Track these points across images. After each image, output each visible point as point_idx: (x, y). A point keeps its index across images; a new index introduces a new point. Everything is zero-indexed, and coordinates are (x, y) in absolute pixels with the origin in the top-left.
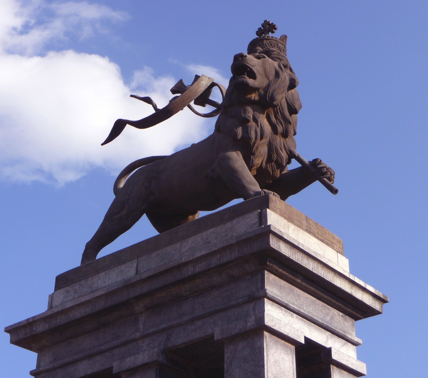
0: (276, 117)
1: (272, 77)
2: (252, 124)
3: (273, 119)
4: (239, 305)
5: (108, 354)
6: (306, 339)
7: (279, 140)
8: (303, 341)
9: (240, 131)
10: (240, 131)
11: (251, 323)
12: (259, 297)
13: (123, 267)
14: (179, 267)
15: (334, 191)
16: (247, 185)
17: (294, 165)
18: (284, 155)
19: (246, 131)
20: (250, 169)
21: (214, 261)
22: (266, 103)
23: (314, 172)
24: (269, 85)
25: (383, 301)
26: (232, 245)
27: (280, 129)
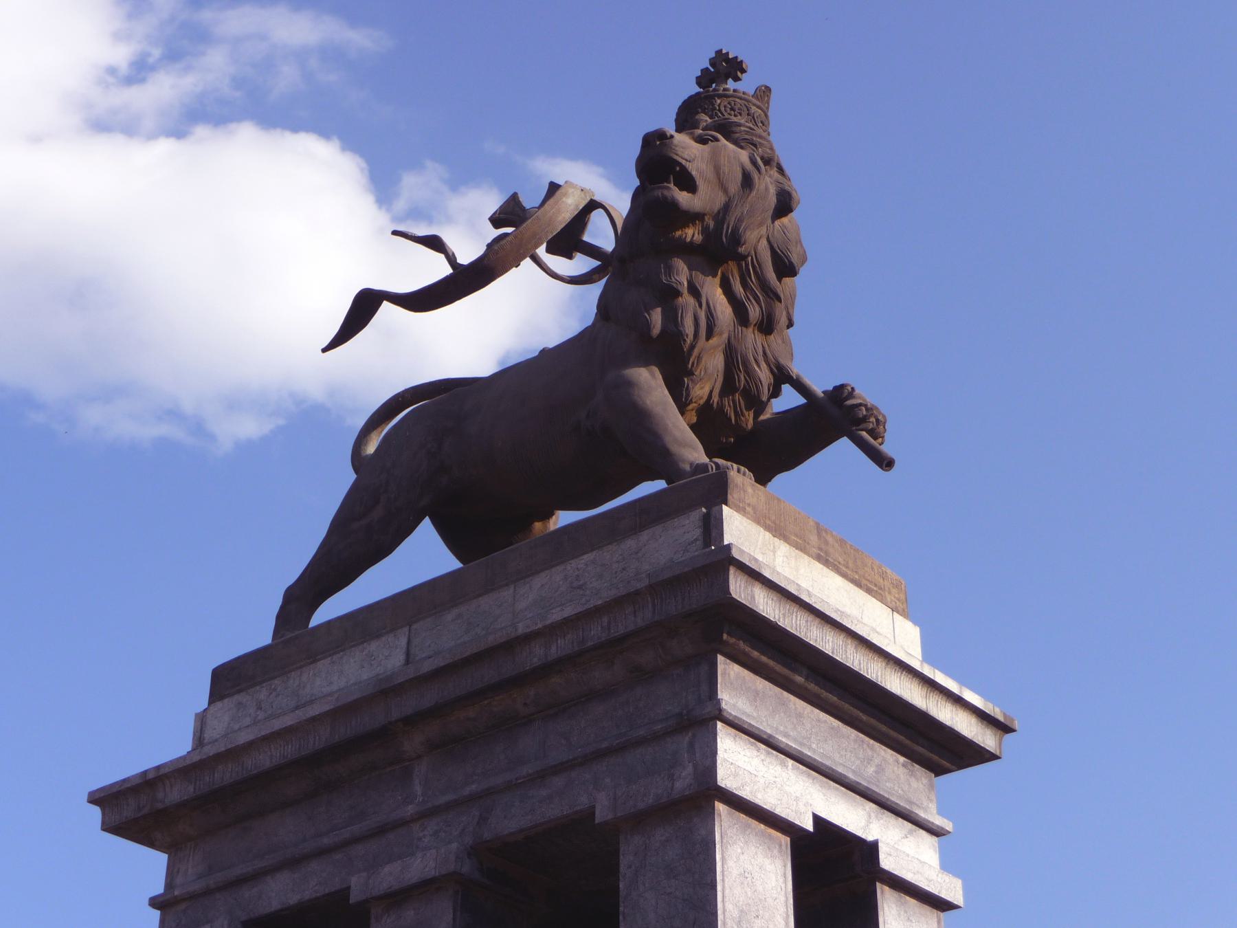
0: (744, 284)
1: (734, 186)
2: (687, 300)
3: (738, 289)
4: (656, 738)
5: (338, 856)
6: (817, 819)
7: (752, 340)
8: (809, 825)
9: (656, 318)
10: (656, 318)
11: (684, 781)
12: (703, 719)
13: (373, 646)
14: (510, 646)
15: (885, 463)
16: (674, 448)
17: (789, 399)
18: (764, 375)
19: (672, 316)
20: (682, 408)
21: (596, 632)
22: (720, 250)
23: (837, 418)
24: (726, 208)
25: (1002, 727)
26: (637, 593)
27: (754, 312)
